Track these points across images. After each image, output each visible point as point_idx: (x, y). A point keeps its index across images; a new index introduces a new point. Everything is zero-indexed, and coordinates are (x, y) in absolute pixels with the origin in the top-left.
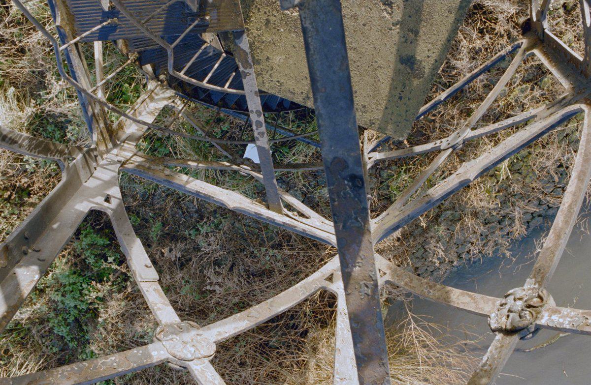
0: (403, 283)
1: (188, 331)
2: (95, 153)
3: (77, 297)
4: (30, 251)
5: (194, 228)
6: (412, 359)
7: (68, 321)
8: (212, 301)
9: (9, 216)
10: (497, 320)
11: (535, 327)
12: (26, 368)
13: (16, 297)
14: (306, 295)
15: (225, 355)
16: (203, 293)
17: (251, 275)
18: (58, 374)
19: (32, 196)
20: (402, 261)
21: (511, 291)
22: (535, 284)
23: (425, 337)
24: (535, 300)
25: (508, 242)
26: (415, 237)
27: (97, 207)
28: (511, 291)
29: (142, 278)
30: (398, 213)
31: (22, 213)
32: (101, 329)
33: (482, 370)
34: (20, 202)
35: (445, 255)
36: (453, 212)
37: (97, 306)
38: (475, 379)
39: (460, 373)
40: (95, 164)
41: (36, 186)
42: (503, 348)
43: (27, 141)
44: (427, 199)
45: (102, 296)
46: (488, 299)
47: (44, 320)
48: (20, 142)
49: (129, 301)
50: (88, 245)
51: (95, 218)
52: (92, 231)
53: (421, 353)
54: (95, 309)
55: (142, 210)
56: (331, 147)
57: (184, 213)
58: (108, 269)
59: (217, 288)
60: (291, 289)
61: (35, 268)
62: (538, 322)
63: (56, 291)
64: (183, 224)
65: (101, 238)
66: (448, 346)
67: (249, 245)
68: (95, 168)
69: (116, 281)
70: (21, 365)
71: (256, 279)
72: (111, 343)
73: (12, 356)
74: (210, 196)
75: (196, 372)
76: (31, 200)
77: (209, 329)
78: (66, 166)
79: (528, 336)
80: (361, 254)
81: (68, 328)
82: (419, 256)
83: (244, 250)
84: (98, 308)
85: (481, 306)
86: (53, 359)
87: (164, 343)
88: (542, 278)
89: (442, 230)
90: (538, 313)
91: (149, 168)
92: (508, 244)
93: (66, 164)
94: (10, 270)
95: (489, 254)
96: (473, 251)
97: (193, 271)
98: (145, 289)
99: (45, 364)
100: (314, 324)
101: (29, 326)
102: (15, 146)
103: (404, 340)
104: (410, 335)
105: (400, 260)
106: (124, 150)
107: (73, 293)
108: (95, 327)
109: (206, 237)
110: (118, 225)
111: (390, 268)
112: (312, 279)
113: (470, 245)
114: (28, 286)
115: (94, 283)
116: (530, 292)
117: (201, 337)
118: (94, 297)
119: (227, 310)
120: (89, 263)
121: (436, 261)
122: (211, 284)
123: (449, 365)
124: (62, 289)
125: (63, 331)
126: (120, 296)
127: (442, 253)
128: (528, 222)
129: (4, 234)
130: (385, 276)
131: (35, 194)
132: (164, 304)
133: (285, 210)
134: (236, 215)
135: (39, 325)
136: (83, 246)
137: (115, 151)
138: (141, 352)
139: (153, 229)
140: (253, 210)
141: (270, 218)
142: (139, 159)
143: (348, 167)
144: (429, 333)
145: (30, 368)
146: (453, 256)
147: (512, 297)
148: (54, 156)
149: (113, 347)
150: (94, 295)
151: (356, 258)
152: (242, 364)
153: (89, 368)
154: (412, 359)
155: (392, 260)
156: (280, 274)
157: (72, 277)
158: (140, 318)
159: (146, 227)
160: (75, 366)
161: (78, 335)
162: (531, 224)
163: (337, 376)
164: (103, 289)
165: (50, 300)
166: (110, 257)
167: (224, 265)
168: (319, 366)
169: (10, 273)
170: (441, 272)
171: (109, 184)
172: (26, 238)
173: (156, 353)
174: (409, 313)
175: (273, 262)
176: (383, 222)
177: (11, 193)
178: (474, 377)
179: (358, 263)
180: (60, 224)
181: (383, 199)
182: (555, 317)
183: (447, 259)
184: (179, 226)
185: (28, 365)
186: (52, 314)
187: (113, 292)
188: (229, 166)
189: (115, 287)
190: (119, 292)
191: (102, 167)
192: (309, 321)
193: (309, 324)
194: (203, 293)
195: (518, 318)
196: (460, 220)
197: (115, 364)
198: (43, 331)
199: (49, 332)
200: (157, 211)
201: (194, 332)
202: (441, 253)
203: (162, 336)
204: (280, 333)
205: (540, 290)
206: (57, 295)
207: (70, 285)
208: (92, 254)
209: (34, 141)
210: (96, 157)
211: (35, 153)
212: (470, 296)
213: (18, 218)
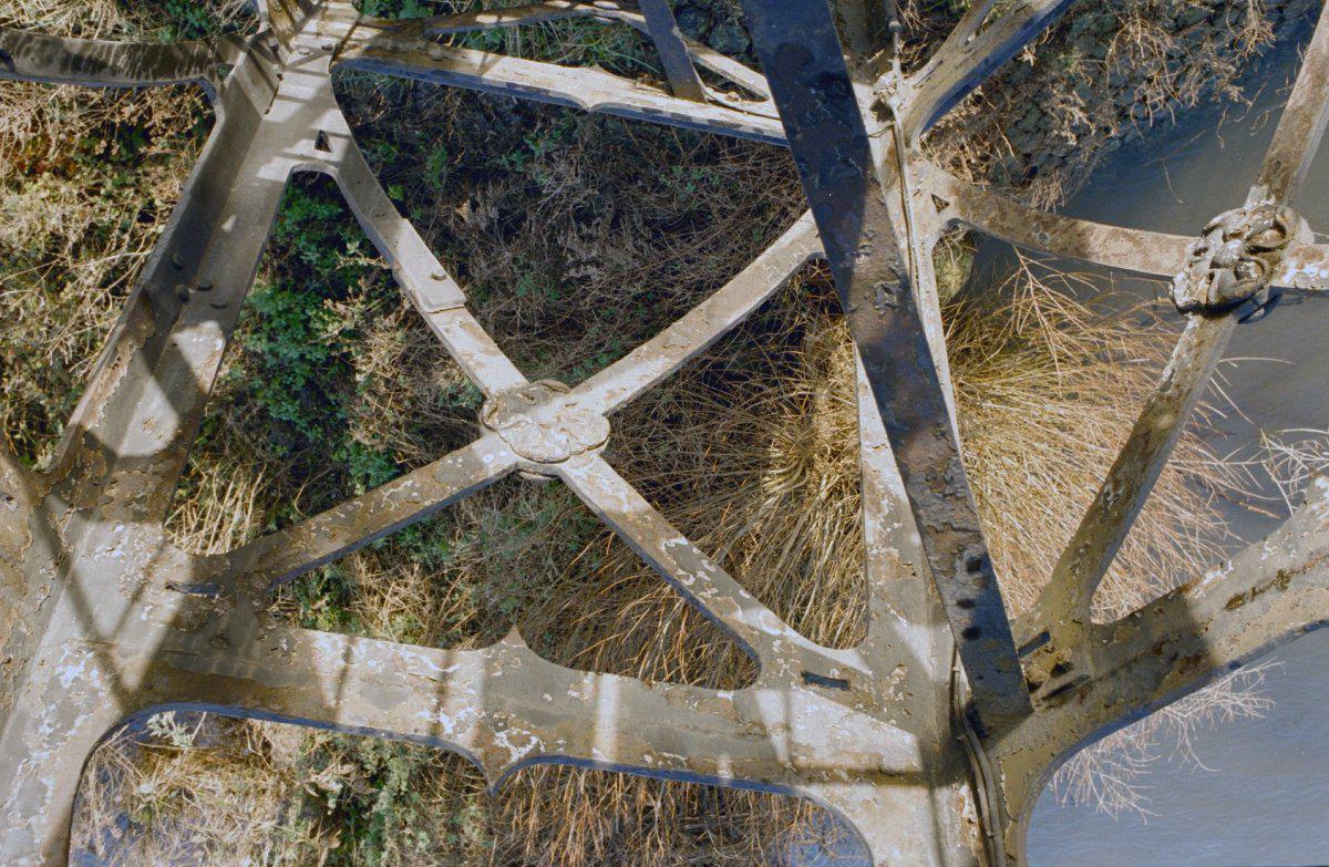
0: (985, 222)
1: (546, 398)
2: (272, 41)
3: (299, 337)
4: (191, 291)
5: (518, 147)
6: (1039, 356)
7: (294, 388)
8: (587, 300)
9: (116, 191)
10: (1189, 288)
11: (1270, 294)
12: (231, 496)
13: (190, 393)
14: (781, 280)
15: (636, 438)
16: (565, 287)
17: (660, 231)
18: (310, 531)
19: (153, 139)
20: (992, 146)
21: (1216, 220)
22: (1268, 198)
23: (1063, 305)
24: (1269, 234)
25: (1233, 63)
26: (1015, 87)
27: (302, 165)
28: (1216, 220)
29: (431, 305)
30: (963, 57)
31: (143, 179)
32: (366, 395)
33: (1161, 398)
34: (130, 156)
35: (1090, 119)
36: (1099, 14)
37: (345, 349)
38: (1149, 418)
39: (1145, 372)
40: (276, 66)
41: (157, 118)
42: (1205, 347)
43: (124, 57)
44: (1024, 17)
45: (352, 327)
46: (1169, 242)
47: (244, 395)
48: (111, 63)
49: (410, 328)
50: (298, 224)
51: (307, 184)
52: (298, 191)
53: (1056, 341)
54: (344, 355)
55: (396, 127)
56: (770, 23)
57: (489, 118)
58: (352, 267)
59: (591, 270)
60: (747, 271)
61: (211, 326)
62: (1275, 283)
63: (255, 332)
64: (491, 142)
65: (321, 202)
66: (1115, 317)
67: (645, 165)
68: (280, 77)
69: (374, 290)
70: (222, 492)
71: (673, 236)
72: (392, 420)
73: (199, 477)
74: (539, 90)
75: (579, 483)
76: (155, 150)
77: (589, 388)
78: (218, 89)
79: (1256, 314)
80: (865, 230)
81: (298, 402)
82: (1030, 128)
83: (637, 176)
84: (349, 353)
85: (1153, 258)
86: (282, 470)
87: (503, 435)
88: (1284, 182)
89: (1075, 62)
90: (1275, 262)
91: (395, 50)
92: (1234, 70)
93: (217, 83)
94: (163, 339)
95: (1190, 99)
96: (1152, 98)
97: (533, 242)
98: (441, 328)
99: (268, 482)
100: (814, 315)
101: (217, 411)
102: (104, 75)
103: (1016, 319)
104: (1027, 305)
105: (987, 144)
106: (332, 18)
107: (289, 331)
108: (353, 393)
109: (548, 165)
110: (357, 198)
111: (956, 191)
112: (790, 239)
113: (1144, 86)
114: (209, 365)
115: (329, 302)
116: (1257, 217)
117: (576, 409)
118: (336, 332)
119: (622, 312)
120: (310, 262)
121: (1069, 134)
122: (578, 264)
123: (1120, 359)
124: (265, 326)
125: (288, 410)
126: (390, 321)
127: (1081, 114)
128: (1280, 9)
129: (117, 232)
130: (947, 209)
131: (157, 135)
132: (487, 351)
133: (709, 92)
134: (607, 119)
135: (237, 405)
136: (289, 229)
137: (312, 25)
138: (460, 460)
139: (429, 166)
140: (638, 105)
141: (679, 115)
142: (368, 34)
143: (812, 59)
144: (1070, 295)
145: (241, 495)
146: (1107, 114)
147: (1219, 233)
148: (187, 74)
149: (398, 426)
150: (334, 329)
151: (856, 239)
152: (674, 421)
153: (366, 509)
154: (1040, 357)
155: (967, 148)
156: (724, 217)
157: (280, 296)
158: (442, 360)
159: (414, 162)
160: (338, 512)
161: (321, 414)
162: (1288, 13)
163: (868, 443)
164: (350, 312)
165: (246, 352)
166: (350, 240)
167: (599, 219)
168: (837, 401)
169: (166, 347)
170: (1084, 158)
171: (314, 107)
172: (179, 268)
173: (491, 457)
174: (1021, 257)
175: (705, 194)
176: (931, 83)
177: (109, 143)
178: (1144, 414)
179: (863, 247)
180: (237, 221)
181: (933, 11)
182: (1311, 269)
183: (1093, 127)
184: (484, 148)
185: (234, 490)
186: (258, 382)
187: (374, 315)
188: (568, 9)
189: (375, 302)
190: (387, 311)
191: (294, 68)
192: (803, 310)
193: (804, 315)
194: (565, 287)
195: (1232, 279)
196: (1117, 30)
197: (415, 494)
198: (247, 417)
199: (261, 417)
200: (431, 124)
201: (558, 402)
202: (1078, 115)
203: (497, 421)
204: (744, 342)
205: (1279, 211)
206: (259, 339)
207: (280, 314)
208: (310, 241)
209: (140, 53)
210: (275, 49)
211: (147, 77)
212: (1130, 238)
213: (137, 192)
